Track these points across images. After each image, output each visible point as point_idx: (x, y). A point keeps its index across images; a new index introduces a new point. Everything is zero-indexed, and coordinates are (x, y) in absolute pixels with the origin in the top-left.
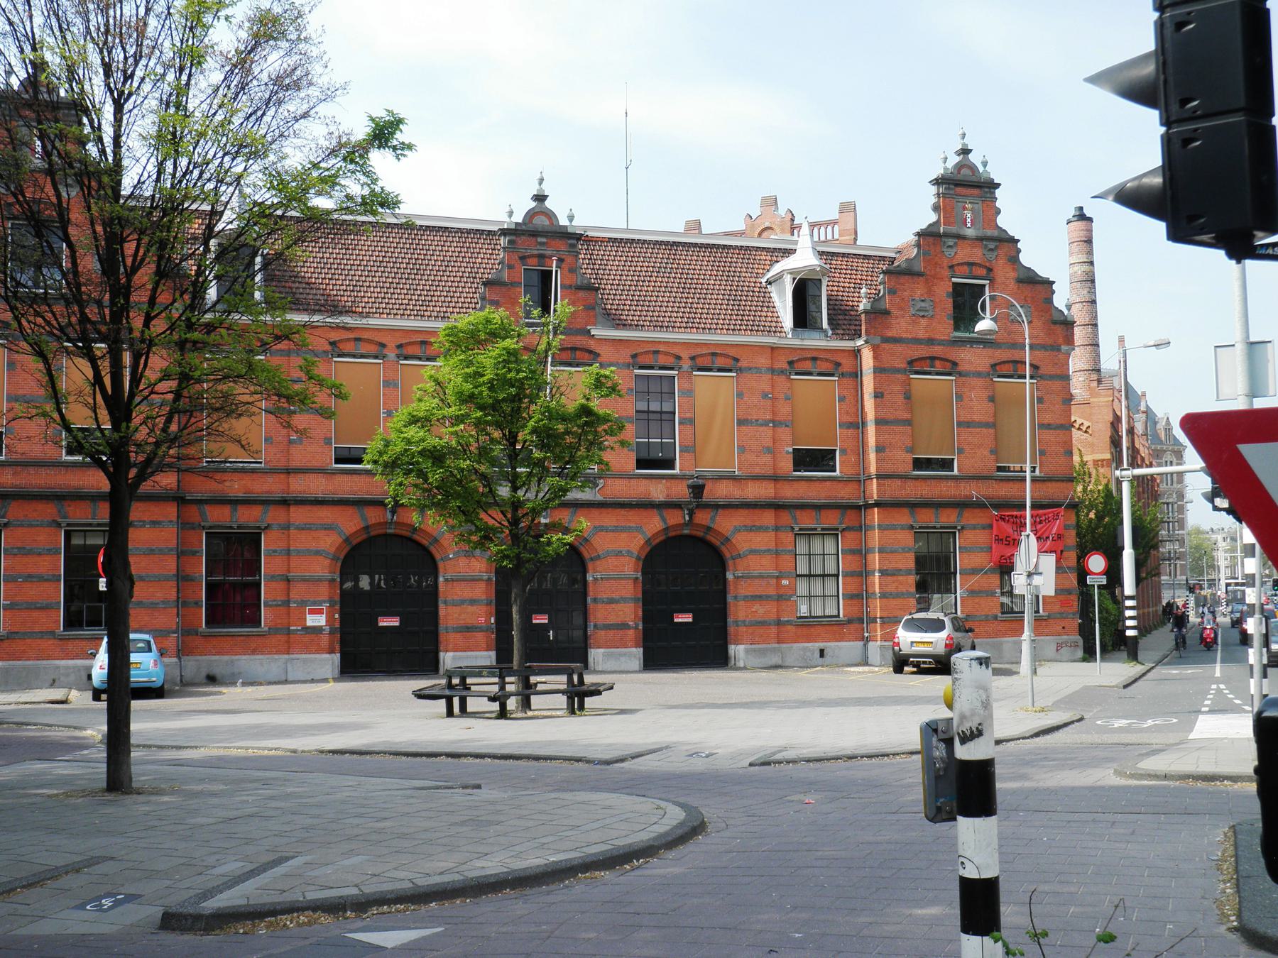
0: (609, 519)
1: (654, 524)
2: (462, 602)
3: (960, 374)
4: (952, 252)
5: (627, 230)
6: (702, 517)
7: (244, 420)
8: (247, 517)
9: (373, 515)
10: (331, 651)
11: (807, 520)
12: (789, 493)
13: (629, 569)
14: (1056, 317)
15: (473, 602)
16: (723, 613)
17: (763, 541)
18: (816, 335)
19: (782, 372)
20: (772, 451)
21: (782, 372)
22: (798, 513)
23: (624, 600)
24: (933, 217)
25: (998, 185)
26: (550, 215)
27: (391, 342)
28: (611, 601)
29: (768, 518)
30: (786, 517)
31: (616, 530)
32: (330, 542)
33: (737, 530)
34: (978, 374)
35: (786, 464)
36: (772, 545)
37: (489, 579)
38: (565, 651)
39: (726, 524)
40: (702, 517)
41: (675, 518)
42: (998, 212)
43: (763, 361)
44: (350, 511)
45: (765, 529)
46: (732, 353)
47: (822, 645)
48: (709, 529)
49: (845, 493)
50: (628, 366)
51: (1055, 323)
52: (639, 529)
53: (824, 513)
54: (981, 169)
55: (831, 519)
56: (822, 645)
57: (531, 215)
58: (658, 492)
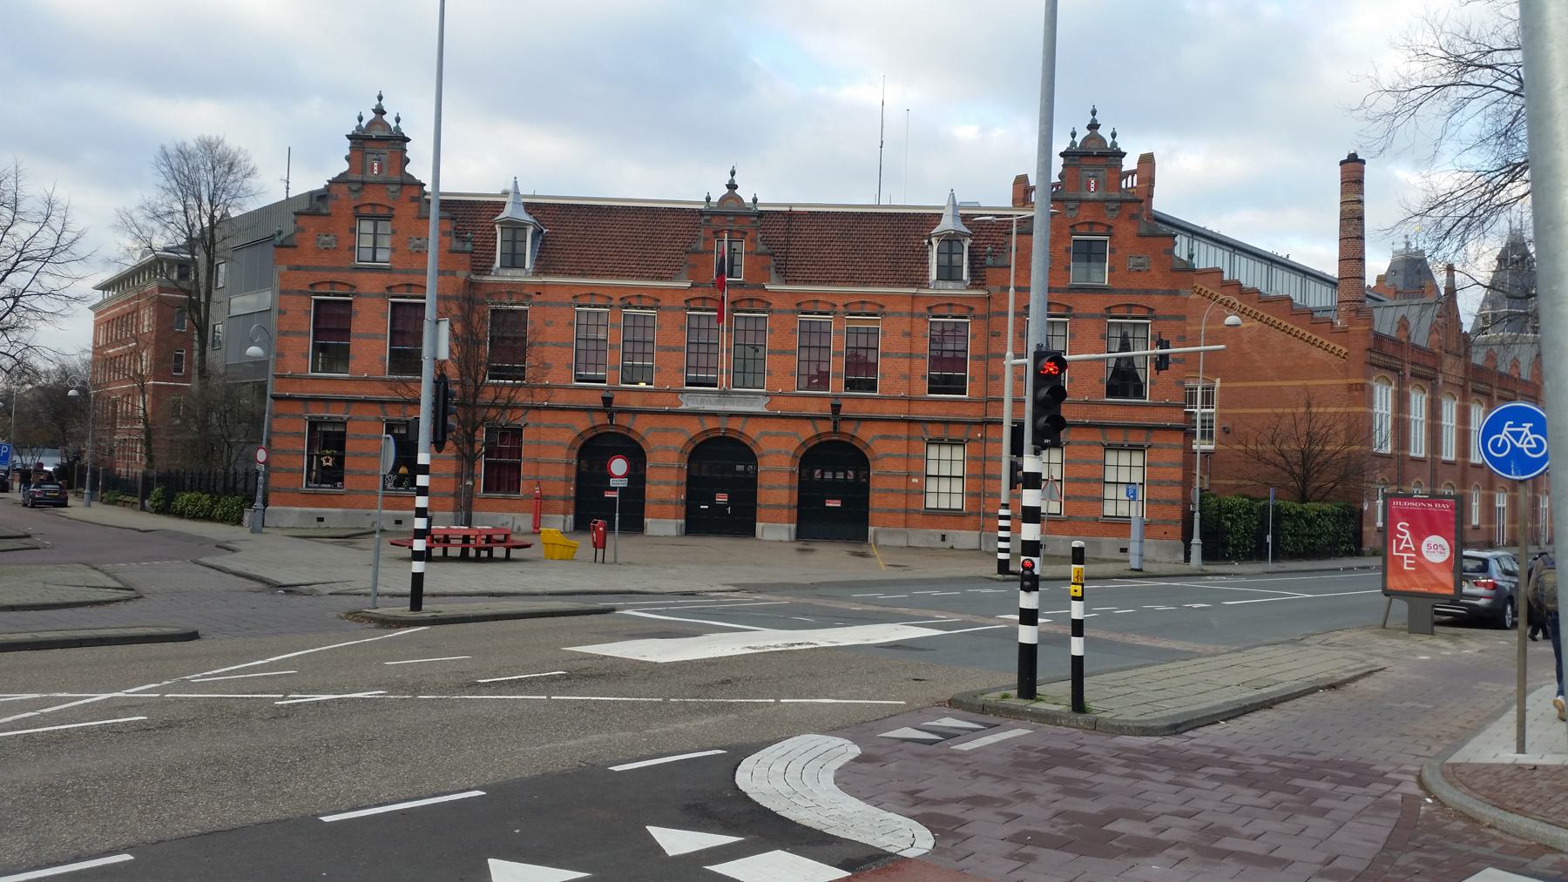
0: (773, 427)
1: (808, 431)
2: (659, 483)
3: (1074, 316)
4: (1074, 214)
5: (879, 206)
6: (846, 428)
7: (31, 332)
8: (337, 413)
9: (710, 424)
10: (566, 513)
11: (1117, 438)
12: (920, 411)
13: (673, 458)
14: (1177, 265)
15: (667, 483)
16: (753, 496)
17: (898, 447)
18: (959, 285)
19: (921, 315)
20: (908, 378)
21: (921, 315)
22: (929, 426)
23: (780, 487)
24: (345, 166)
25: (378, 142)
26: (739, 199)
27: (839, 303)
28: (772, 488)
29: (902, 430)
30: (918, 430)
31: (777, 435)
32: (568, 437)
33: (874, 438)
34: (1092, 316)
35: (921, 388)
36: (904, 451)
37: (792, 473)
38: (738, 521)
39: (866, 434)
40: (846, 428)
41: (826, 427)
42: (408, 161)
43: (905, 308)
44: (583, 415)
45: (900, 438)
46: (878, 301)
47: (943, 532)
48: (629, 430)
49: (973, 413)
50: (681, 309)
51: (1174, 270)
52: (795, 435)
53: (952, 427)
54: (1109, 141)
55: (1135, 438)
56: (943, 532)
57: (723, 199)
58: (813, 408)
